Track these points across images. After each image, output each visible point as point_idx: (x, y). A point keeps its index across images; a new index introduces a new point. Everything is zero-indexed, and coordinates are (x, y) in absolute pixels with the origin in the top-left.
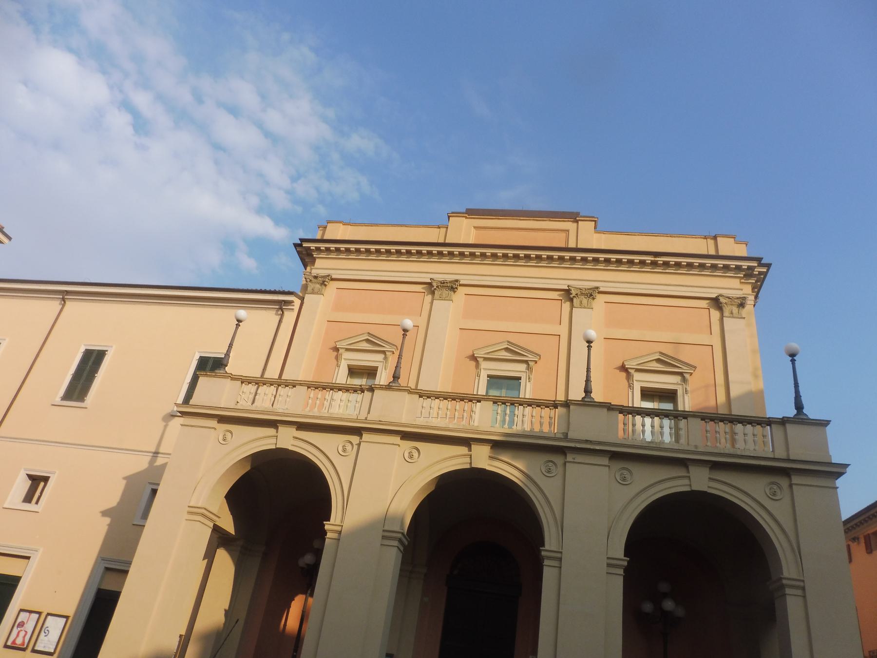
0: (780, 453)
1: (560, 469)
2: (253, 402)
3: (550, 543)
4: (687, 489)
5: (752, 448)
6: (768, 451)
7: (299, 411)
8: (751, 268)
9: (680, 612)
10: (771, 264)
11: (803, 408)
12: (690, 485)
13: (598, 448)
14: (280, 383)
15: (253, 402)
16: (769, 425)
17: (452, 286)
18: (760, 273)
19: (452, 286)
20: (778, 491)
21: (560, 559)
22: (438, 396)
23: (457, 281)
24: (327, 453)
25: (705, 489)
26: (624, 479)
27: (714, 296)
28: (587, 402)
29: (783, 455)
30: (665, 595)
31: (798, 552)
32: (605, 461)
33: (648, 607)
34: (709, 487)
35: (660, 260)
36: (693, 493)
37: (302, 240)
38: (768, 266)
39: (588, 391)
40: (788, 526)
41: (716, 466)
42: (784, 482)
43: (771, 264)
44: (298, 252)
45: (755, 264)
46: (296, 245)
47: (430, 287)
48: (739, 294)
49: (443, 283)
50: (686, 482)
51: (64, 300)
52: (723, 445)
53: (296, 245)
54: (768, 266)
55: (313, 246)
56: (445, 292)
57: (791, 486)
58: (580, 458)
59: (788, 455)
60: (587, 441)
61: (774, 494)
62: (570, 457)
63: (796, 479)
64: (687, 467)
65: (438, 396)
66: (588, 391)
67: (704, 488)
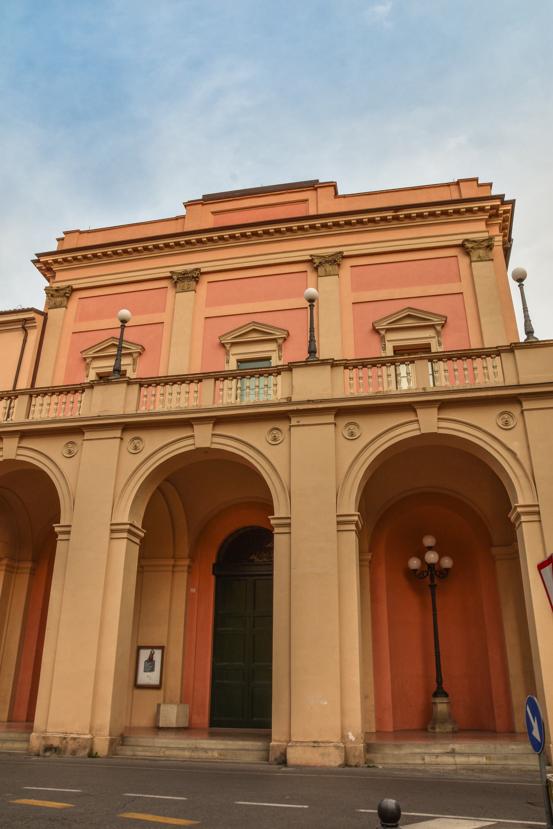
0: (511, 381)
1: (520, 419)
2: (8, 416)
3: (522, 497)
4: (417, 433)
5: (233, 402)
6: (498, 381)
7: (327, 395)
8: (493, 208)
9: (447, 563)
10: (514, 200)
11: (533, 332)
12: (420, 429)
13: (320, 406)
14: (33, 392)
15: (8, 416)
16: (499, 355)
17: (336, 260)
18: (506, 212)
19: (336, 260)
20: (510, 420)
21: (538, 513)
22: (347, 365)
23: (197, 269)
24: (252, 444)
25: (435, 430)
26: (352, 434)
27: (460, 242)
28: (532, 344)
29: (514, 382)
30: (430, 548)
31: (532, 479)
32: (330, 419)
33: (414, 563)
34: (438, 428)
35: (402, 214)
36: (423, 436)
37: (38, 255)
38: (512, 202)
39: (529, 332)
40: (521, 454)
41: (444, 405)
42: (515, 410)
43: (514, 200)
44: (40, 269)
45: (498, 203)
46: (34, 262)
47: (465, 248)
48: (486, 235)
49: (185, 273)
50: (415, 426)
51: (25, 329)
52: (207, 402)
53: (34, 262)
54: (512, 202)
55: (50, 259)
56: (329, 268)
57: (522, 412)
58: (304, 420)
59: (518, 382)
60: (309, 402)
61: (507, 423)
62: (294, 421)
63: (526, 405)
64: (415, 411)
65: (347, 365)
66: (529, 332)
67: (207, 445)
